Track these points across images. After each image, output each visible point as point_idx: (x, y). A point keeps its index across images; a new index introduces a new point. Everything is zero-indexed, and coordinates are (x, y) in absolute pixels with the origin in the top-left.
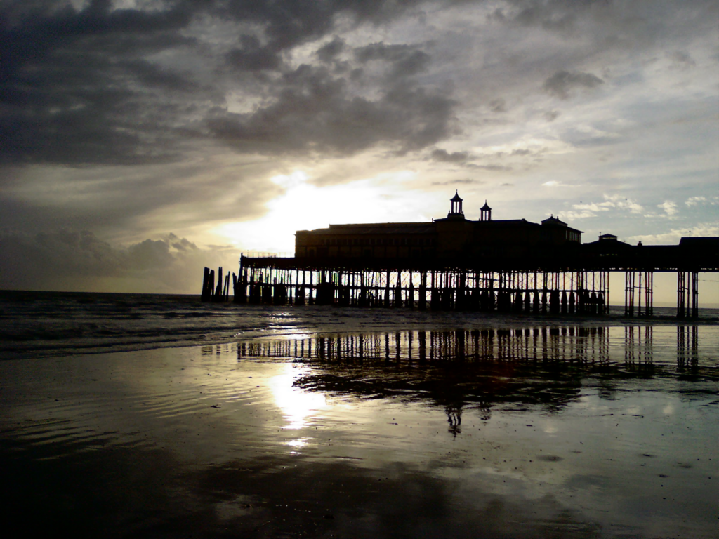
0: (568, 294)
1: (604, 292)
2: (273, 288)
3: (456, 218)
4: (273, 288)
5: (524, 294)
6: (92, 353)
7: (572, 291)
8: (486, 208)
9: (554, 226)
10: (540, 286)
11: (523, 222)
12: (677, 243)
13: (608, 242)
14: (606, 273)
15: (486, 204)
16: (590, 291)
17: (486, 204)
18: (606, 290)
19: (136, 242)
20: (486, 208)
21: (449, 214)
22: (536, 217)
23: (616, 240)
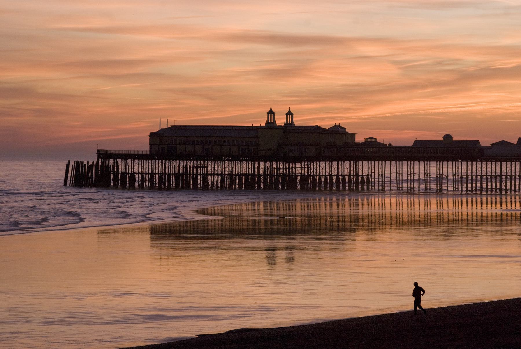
0: (347, 178)
1: (371, 175)
2: (244, 177)
3: (271, 126)
4: (244, 177)
5: (318, 178)
6: (502, 262)
7: (350, 176)
8: (289, 114)
9: (338, 131)
10: (334, 172)
11: (317, 128)
12: (411, 144)
13: (371, 143)
14: (428, 162)
15: (289, 110)
16: (298, 176)
17: (289, 110)
18: (373, 174)
19: (228, 116)
20: (289, 114)
21: (266, 124)
22: (326, 124)
23: (376, 141)
